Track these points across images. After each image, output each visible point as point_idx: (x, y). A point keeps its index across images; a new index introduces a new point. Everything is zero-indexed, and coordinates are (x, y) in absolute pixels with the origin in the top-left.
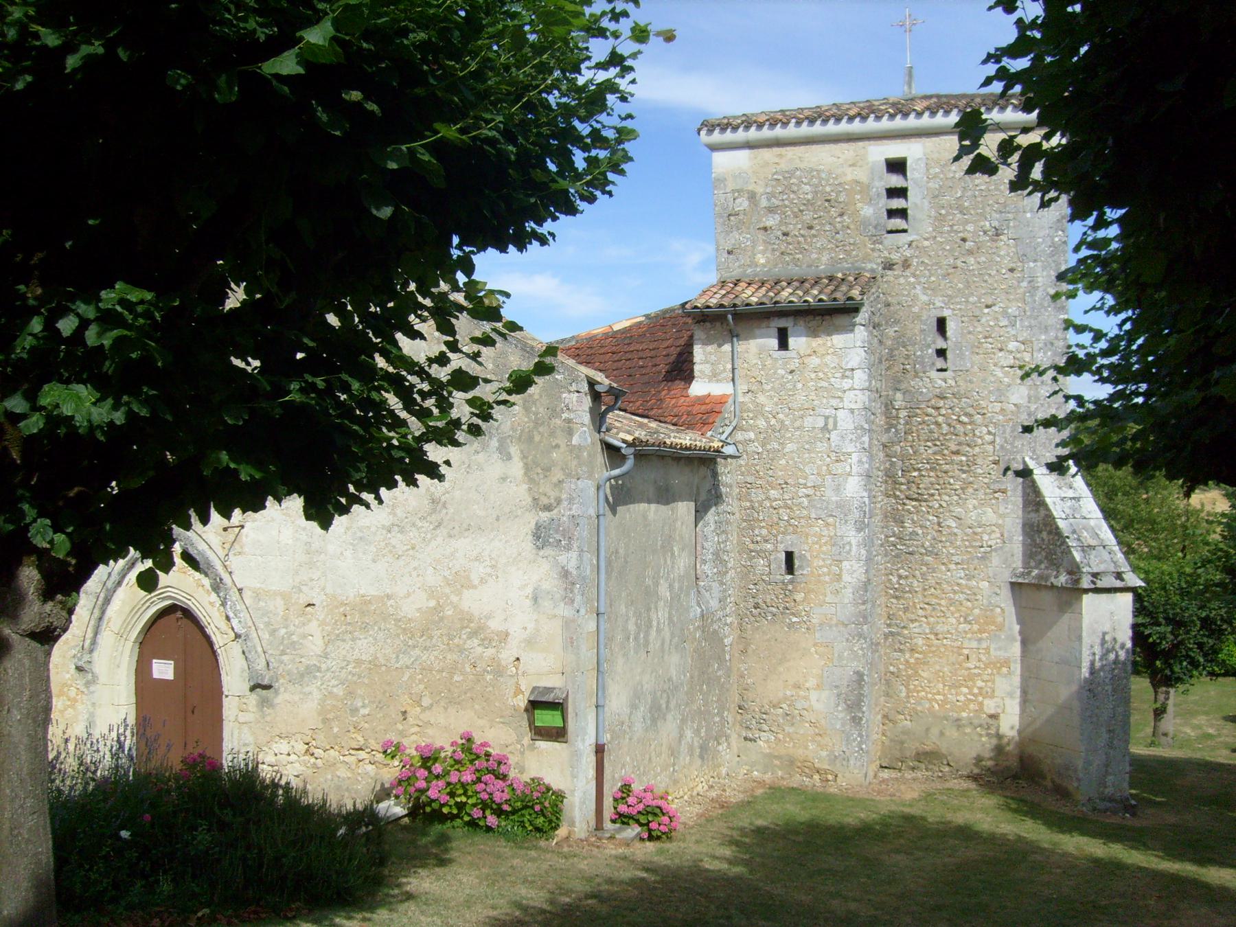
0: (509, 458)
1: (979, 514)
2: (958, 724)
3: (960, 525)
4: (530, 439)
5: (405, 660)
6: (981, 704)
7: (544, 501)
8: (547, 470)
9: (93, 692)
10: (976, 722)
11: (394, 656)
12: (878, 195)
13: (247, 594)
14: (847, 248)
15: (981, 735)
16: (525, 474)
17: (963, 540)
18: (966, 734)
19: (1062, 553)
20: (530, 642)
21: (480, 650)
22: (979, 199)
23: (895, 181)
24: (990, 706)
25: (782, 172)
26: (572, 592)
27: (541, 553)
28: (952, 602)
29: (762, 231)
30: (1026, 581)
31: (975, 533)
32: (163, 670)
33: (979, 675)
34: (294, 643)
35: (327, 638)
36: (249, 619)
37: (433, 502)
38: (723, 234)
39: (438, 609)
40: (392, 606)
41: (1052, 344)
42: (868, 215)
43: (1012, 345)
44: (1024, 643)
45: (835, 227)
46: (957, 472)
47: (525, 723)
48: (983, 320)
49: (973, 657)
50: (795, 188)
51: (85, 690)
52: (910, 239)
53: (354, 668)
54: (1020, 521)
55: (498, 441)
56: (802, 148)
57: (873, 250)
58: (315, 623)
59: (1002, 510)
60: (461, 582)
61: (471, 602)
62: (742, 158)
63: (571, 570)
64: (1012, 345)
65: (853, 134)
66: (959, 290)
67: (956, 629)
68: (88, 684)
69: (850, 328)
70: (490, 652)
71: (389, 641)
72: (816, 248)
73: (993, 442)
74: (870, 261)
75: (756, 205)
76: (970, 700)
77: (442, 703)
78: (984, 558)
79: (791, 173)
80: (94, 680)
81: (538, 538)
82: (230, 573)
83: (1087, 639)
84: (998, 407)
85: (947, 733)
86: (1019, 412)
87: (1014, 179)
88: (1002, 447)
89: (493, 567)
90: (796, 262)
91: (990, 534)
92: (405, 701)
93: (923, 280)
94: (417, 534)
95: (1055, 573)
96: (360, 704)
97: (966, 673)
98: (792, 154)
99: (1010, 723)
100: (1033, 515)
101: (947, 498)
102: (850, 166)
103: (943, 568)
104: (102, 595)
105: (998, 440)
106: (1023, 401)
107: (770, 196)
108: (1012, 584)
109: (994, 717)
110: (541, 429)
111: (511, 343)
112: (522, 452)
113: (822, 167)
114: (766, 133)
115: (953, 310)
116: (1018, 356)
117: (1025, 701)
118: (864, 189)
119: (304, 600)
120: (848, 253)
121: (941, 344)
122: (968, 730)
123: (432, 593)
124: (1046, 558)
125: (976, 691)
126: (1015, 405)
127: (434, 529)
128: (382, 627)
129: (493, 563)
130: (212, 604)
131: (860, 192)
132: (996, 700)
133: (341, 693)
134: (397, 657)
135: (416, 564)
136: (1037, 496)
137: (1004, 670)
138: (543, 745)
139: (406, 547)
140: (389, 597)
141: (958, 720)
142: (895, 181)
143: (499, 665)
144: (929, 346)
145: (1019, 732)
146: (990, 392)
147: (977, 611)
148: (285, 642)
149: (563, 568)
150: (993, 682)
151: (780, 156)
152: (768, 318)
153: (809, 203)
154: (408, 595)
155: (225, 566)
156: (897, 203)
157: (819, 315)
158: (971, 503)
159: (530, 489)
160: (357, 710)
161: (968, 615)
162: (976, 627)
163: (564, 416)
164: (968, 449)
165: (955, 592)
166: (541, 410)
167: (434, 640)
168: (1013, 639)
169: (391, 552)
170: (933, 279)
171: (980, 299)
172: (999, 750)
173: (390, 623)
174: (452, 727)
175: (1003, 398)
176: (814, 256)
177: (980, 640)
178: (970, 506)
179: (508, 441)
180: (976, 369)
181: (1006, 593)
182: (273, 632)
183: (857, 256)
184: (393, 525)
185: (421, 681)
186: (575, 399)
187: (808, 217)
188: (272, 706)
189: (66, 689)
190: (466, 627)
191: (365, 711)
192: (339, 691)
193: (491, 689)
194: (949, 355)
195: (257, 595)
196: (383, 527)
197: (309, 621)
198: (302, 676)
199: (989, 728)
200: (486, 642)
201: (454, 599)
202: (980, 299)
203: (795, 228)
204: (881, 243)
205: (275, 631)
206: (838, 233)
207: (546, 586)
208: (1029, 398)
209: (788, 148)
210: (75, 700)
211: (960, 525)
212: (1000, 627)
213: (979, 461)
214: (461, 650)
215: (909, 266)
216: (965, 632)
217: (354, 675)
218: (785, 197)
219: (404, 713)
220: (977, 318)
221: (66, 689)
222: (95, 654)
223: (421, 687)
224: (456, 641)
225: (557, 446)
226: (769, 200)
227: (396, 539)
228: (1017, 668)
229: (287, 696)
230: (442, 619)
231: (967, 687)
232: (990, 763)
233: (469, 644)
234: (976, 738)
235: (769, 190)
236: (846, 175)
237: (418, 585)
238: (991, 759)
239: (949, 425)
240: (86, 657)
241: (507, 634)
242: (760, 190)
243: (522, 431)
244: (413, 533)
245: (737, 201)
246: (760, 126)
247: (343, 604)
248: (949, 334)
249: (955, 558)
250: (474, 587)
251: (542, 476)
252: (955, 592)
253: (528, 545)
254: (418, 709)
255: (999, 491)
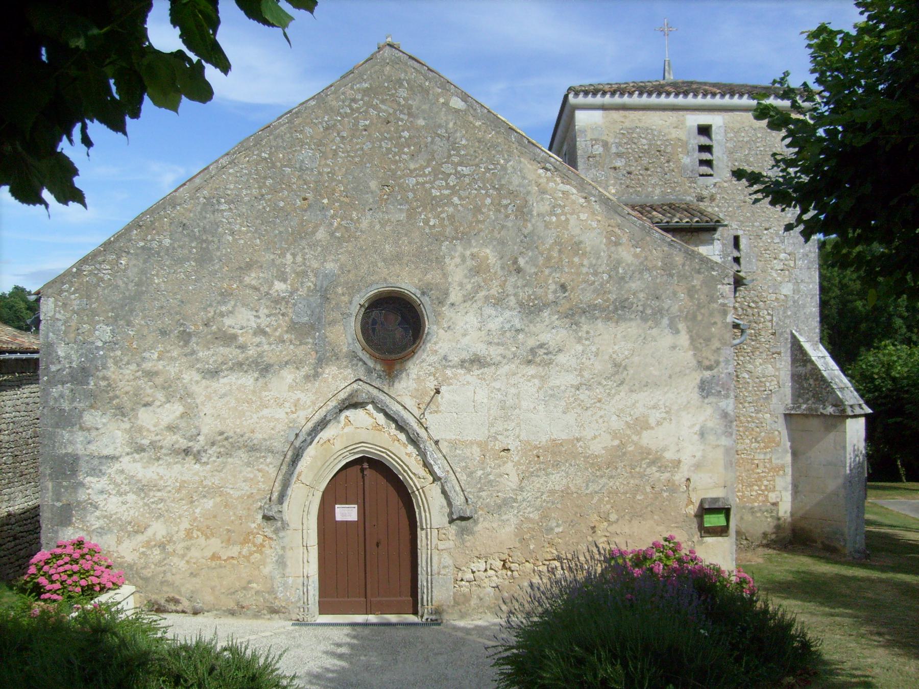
0: (678, 332)
1: (763, 369)
2: (752, 511)
3: (752, 376)
4: (694, 318)
5: (593, 487)
6: (767, 496)
7: (707, 363)
8: (708, 340)
9: (283, 537)
10: (764, 508)
11: (584, 484)
12: (693, 149)
13: (443, 446)
14: (673, 185)
15: (767, 517)
16: (691, 343)
17: (753, 387)
18: (757, 517)
19: (827, 393)
20: (698, 466)
21: (658, 474)
22: (760, 157)
23: (704, 141)
24: (772, 497)
25: (627, 129)
26: (730, 427)
27: (706, 401)
28: (746, 428)
29: (613, 170)
30: (799, 412)
31: (761, 382)
32: (347, 513)
33: (765, 477)
34: (490, 482)
35: (522, 476)
36: (447, 464)
37: (615, 366)
38: (584, 171)
39: (622, 445)
40: (581, 447)
41: (807, 255)
42: (686, 163)
43: (782, 256)
44: (795, 454)
45: (664, 170)
46: (749, 341)
47: (695, 525)
48: (764, 238)
49: (761, 465)
50: (636, 141)
51: (274, 537)
52: (715, 181)
53: (549, 496)
54: (789, 373)
55: (669, 319)
56: (641, 112)
57: (690, 187)
58: (510, 465)
59: (778, 366)
60: (641, 424)
61: (648, 439)
62: (597, 115)
63: (730, 412)
64: (782, 256)
65: (677, 106)
66: (748, 217)
67: (750, 447)
68: (276, 531)
69: (711, 242)
70: (667, 475)
71: (579, 473)
72: (651, 184)
73: (771, 321)
74: (689, 195)
75: (608, 151)
76: (760, 494)
77: (627, 517)
78: (768, 398)
79: (633, 129)
80: (285, 526)
81: (703, 390)
82: (426, 429)
83: (849, 449)
84: (773, 297)
85: (745, 518)
86: (787, 300)
87: (96, 129)
88: (777, 323)
89: (667, 412)
90: (637, 193)
91: (770, 382)
92: (594, 518)
93: (724, 210)
94: (602, 390)
95: (821, 406)
96: (555, 524)
97: (756, 476)
98: (634, 117)
99: (785, 508)
100: (800, 369)
101: (742, 358)
102: (674, 128)
103: (741, 406)
104: (290, 454)
105: (774, 319)
106: (789, 293)
107: (618, 145)
108: (785, 415)
109: (775, 504)
110: (702, 311)
111: (676, 248)
112: (688, 327)
113: (654, 127)
114: (617, 100)
115: (744, 230)
116: (786, 263)
117: (796, 490)
118: (685, 144)
119: (498, 446)
120: (673, 189)
121: (736, 254)
122: (759, 514)
123: (615, 435)
124: (813, 396)
125: (763, 488)
126: (785, 295)
127: (617, 386)
128: (573, 464)
129: (667, 409)
130: (409, 455)
131: (681, 147)
132: (777, 493)
133: (537, 518)
134: (587, 485)
135: (602, 413)
136: (803, 356)
137: (781, 472)
138: (709, 540)
139: (593, 401)
140: (578, 440)
141: (752, 508)
142: (704, 141)
143: (674, 484)
144: (729, 255)
145: (792, 515)
146: (769, 287)
147: (763, 434)
148: (482, 481)
149: (723, 411)
150: (774, 481)
151: (625, 117)
152: (692, 232)
153: (645, 152)
154: (595, 437)
155: (421, 423)
156: (706, 156)
157: (689, 232)
158: (758, 361)
159: (695, 355)
160: (552, 529)
161: (757, 437)
162: (762, 445)
163: (720, 301)
164: (755, 325)
165: (748, 422)
166: (702, 297)
167: (619, 470)
168: (787, 452)
169: (580, 405)
170: (730, 209)
171: (761, 224)
172: (778, 527)
173: (580, 460)
174: (635, 534)
175: (777, 291)
176: (650, 189)
177: (765, 454)
178: (758, 364)
179: (677, 319)
180: (759, 271)
181: (781, 420)
182: (470, 474)
183: (680, 191)
184: (581, 384)
185: (608, 502)
186: (727, 290)
187: (645, 161)
188: (471, 533)
189: (251, 537)
190: (646, 459)
191: (560, 529)
192: (535, 516)
193: (667, 503)
194: (742, 261)
195: (454, 445)
196: (572, 386)
197: (505, 463)
198: (500, 507)
199: (772, 512)
200: (662, 469)
201: (635, 438)
202: (761, 224)
203: (636, 169)
204: (695, 183)
205: (472, 473)
206: (666, 174)
207: (710, 424)
208: (794, 291)
209: (631, 112)
210: (262, 546)
211: (752, 376)
212: (778, 445)
213: (763, 333)
214: (642, 476)
215: (714, 200)
216: (756, 449)
217: (548, 502)
218: (629, 146)
219: (593, 528)
220: (759, 237)
221: (251, 537)
222: (285, 505)
223: (608, 506)
224: (637, 469)
225: (715, 323)
226: (617, 148)
227: (584, 395)
228: (789, 470)
229: (486, 524)
230: (624, 454)
231: (758, 486)
232: (773, 537)
233: (648, 471)
234: (764, 519)
235: (617, 141)
236: (671, 134)
237: (604, 429)
238: (774, 533)
239: (743, 309)
240: (275, 508)
241: (679, 462)
242: (610, 140)
243: (688, 312)
244: (599, 390)
245: (594, 147)
246: (604, 93)
247: (536, 447)
248: (742, 247)
249: (748, 399)
250: (652, 428)
251: (704, 345)
252: (748, 422)
253: (695, 396)
254: (605, 524)
255: (776, 353)
